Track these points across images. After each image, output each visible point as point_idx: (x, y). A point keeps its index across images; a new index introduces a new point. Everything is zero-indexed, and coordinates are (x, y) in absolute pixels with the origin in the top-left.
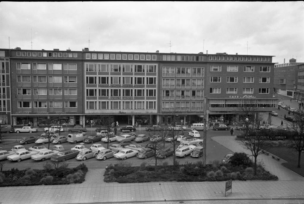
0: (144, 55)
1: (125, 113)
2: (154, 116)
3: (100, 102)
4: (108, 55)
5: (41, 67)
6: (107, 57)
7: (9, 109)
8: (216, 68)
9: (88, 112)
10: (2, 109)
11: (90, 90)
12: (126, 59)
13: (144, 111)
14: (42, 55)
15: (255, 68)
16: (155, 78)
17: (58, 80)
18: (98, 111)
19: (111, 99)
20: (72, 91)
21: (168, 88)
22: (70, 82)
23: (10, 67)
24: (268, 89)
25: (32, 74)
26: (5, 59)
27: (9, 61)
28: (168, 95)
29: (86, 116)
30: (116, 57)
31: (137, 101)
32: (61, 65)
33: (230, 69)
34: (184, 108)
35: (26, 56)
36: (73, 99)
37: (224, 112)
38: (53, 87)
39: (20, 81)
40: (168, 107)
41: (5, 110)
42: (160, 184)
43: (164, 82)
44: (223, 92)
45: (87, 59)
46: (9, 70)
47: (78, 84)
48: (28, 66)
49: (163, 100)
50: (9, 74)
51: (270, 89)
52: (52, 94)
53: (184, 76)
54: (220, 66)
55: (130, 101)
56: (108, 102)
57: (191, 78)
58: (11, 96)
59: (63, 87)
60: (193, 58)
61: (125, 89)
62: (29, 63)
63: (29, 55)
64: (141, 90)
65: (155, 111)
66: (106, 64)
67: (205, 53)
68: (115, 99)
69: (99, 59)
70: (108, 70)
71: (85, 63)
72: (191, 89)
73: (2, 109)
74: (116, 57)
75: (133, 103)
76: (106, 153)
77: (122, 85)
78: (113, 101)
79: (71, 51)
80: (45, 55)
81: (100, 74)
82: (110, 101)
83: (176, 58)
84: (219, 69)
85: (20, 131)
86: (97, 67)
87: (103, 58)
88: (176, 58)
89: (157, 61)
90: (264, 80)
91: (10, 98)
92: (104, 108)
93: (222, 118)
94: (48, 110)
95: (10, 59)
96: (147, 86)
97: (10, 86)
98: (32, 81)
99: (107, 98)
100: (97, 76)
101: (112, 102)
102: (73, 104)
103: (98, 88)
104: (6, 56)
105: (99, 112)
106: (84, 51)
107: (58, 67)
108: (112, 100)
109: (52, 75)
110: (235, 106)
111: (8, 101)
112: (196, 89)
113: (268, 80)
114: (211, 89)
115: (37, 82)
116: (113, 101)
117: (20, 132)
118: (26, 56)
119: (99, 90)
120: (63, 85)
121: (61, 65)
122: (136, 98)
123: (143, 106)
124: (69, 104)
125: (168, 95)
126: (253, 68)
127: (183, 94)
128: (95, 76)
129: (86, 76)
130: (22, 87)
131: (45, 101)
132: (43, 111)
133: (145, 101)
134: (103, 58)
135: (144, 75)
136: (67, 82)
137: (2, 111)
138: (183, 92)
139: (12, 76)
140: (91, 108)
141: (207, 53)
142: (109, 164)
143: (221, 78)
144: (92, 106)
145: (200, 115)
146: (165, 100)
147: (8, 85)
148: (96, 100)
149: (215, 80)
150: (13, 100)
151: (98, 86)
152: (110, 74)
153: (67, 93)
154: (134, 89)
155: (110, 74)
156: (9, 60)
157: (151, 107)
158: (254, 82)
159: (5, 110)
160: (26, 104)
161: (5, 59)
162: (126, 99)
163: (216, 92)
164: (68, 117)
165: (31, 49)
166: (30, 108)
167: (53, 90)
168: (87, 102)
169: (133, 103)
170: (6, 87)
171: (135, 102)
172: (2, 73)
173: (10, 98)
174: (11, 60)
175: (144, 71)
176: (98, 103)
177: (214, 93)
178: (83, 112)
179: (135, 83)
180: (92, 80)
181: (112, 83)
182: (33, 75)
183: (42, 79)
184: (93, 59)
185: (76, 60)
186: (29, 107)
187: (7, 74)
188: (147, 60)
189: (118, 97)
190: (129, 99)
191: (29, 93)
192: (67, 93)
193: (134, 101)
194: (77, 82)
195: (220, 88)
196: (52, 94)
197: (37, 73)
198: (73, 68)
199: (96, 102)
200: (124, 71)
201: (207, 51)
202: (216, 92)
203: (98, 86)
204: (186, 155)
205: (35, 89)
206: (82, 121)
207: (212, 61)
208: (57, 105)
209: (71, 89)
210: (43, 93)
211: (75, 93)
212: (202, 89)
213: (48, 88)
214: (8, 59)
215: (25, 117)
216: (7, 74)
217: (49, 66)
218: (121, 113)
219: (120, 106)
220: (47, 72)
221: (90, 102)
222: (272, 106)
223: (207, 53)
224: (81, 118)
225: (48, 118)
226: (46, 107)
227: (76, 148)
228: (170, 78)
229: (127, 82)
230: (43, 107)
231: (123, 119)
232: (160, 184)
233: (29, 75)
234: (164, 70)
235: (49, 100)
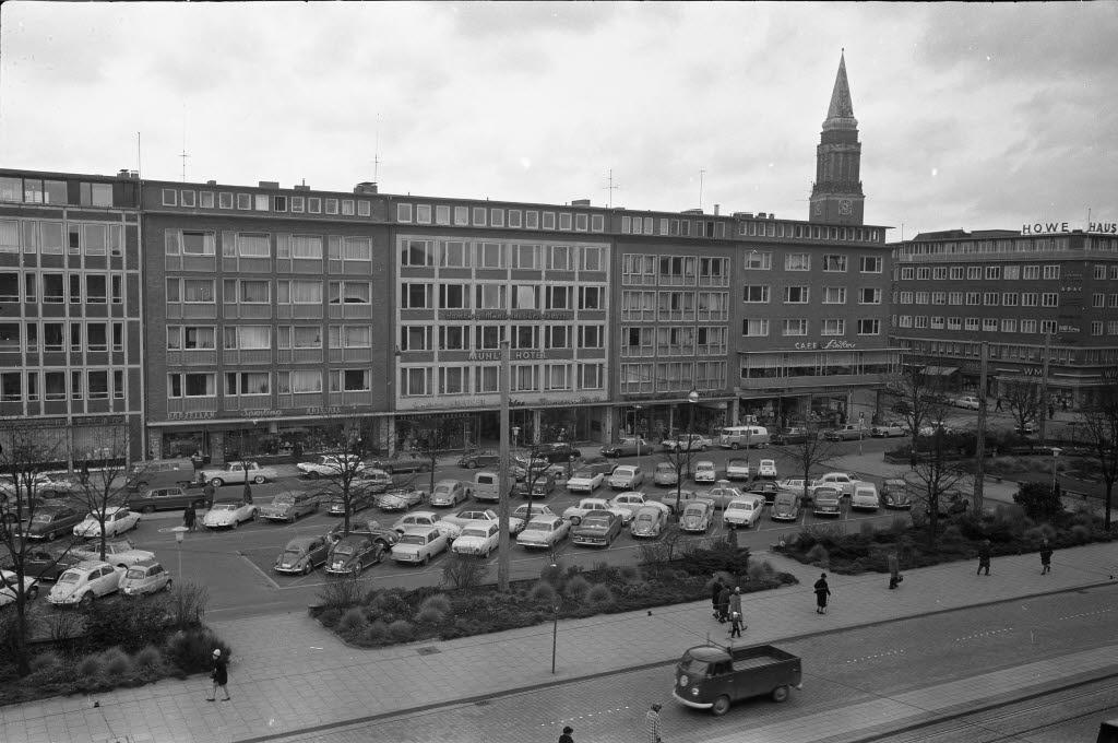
0: (570, 214)
1: (523, 404)
2: (598, 409)
3: (442, 370)
4: (210, 195)
5: (249, 249)
6: (461, 220)
7: (135, 404)
8: (756, 259)
9: (404, 404)
10: (111, 404)
11: (587, 328)
12: (503, 226)
13: (572, 394)
14: (254, 205)
15: (850, 260)
16: (603, 289)
17: (311, 296)
18: (436, 400)
19: (478, 359)
20: (354, 335)
21: (637, 321)
22: (347, 300)
23: (143, 246)
24: (876, 321)
25: (219, 274)
26: (124, 217)
27: (138, 224)
28: (634, 340)
29: (397, 417)
30: (489, 219)
31: (551, 362)
32: (267, 243)
33: (792, 263)
34: (678, 382)
35: (232, 208)
36: (356, 362)
37: (777, 390)
38: (293, 321)
39: (177, 299)
40: (640, 383)
41: (119, 406)
42: (97, 705)
43: (627, 304)
44: (777, 329)
45: (401, 222)
46: (137, 255)
47: (374, 307)
48: (202, 241)
49: (623, 360)
50: (139, 271)
51: (811, 322)
52: (290, 343)
53: (673, 282)
54: (767, 255)
55: (532, 363)
56: (467, 369)
57: (698, 289)
58: (146, 354)
59: (323, 321)
60: (675, 224)
61: (483, 323)
62: (210, 234)
63: (315, 207)
64: (530, 328)
65: (601, 395)
66: (498, 242)
67: (709, 211)
68: (489, 359)
69: (439, 222)
70: (538, 265)
71: (400, 238)
72: (697, 323)
73: (111, 404)
74: (489, 219)
75: (542, 370)
76: (91, 577)
77: (509, 313)
78: (484, 364)
79: (281, 187)
80: (262, 204)
81: (583, 277)
82: (472, 366)
83: (657, 228)
84: (766, 263)
85: (222, 481)
86: (434, 246)
87: (452, 221)
88: (657, 228)
89: (608, 233)
90: (869, 295)
91: (139, 363)
92: (454, 388)
93: (771, 409)
94: (274, 402)
95: (145, 216)
96: (582, 316)
97: (140, 319)
98: (219, 298)
99: (465, 357)
100: (437, 281)
101: (478, 368)
102: (354, 379)
103: (436, 323)
104: (118, 201)
105: (475, 403)
106: (358, 193)
107: (309, 250)
108: (478, 364)
109: (290, 275)
110: (810, 371)
111: (134, 374)
112: (709, 323)
113: (878, 296)
114: (745, 323)
115: (238, 300)
116: (484, 364)
117: (223, 484)
118: (232, 208)
119: (442, 328)
120: (326, 314)
121: (267, 243)
122: (549, 355)
123: (569, 381)
124: (342, 378)
125: (634, 340)
126: (844, 260)
127: (702, 340)
128: (430, 280)
129: (400, 280)
130: (183, 321)
131: (262, 371)
132: (255, 405)
133: (575, 361)
134: (452, 221)
135: (433, 276)
136: (338, 301)
137: (111, 412)
138: (702, 332)
139: (149, 278)
140: (417, 389)
141: (716, 211)
142: (787, 535)
143: (769, 291)
144: (454, 380)
145: (719, 401)
146: (629, 360)
147: (133, 312)
148: (429, 364)
149: (756, 296)
150: (151, 369)
151: (436, 317)
152: (437, 273)
153: (338, 342)
154: (543, 324)
155: (437, 273)
156: (139, 219)
157: (590, 381)
158: (772, 300)
159: (119, 406)
160: (197, 384)
161: (124, 217)
162: (523, 358)
163: (757, 330)
164: (340, 424)
165: (182, 181)
166: (208, 396)
167: (292, 330)
168: (404, 370)
169: (542, 370)
170: (125, 320)
171: (547, 367)
172: (112, 268)
173: (139, 363)
174: (148, 221)
175: (430, 262)
176: (436, 374)
177: (752, 335)
178: (390, 406)
179: (548, 306)
180: (417, 295)
181: (479, 305)
182: (225, 275)
183: (253, 292)
184: (420, 222)
185: (186, 216)
186: (205, 393)
187: (131, 271)
188: (578, 230)
189: (497, 352)
190: (531, 358)
191: (207, 345)
192: (338, 342)
193: (542, 363)
194: (370, 303)
195: (765, 321)
196: (290, 343)
197: (292, 272)
198: (356, 253)
199: (430, 369)
200: (442, 263)
201: (717, 206)
202: (757, 330)
203: (436, 317)
204: (429, 555)
205: (227, 326)
206: (388, 436)
207: (810, 242)
208: (303, 383)
209: (353, 326)
210: (253, 340)
211: (364, 341)
212: (723, 323)
213: (276, 323)
214: (136, 215)
215: (232, 428)
216: (131, 271)
217: (332, 246)
218: (350, 410)
219: (467, 382)
220: (274, 267)
221: (587, 365)
222: (890, 370)
223: (716, 211)
224: (383, 425)
225: (274, 430)
226: (264, 389)
227: (828, 480)
228: (643, 288)
229: (490, 300)
230: (254, 392)
231: (486, 425)
232: (97, 705)
233: (364, 281)
234: (628, 262)
235: (277, 365)
